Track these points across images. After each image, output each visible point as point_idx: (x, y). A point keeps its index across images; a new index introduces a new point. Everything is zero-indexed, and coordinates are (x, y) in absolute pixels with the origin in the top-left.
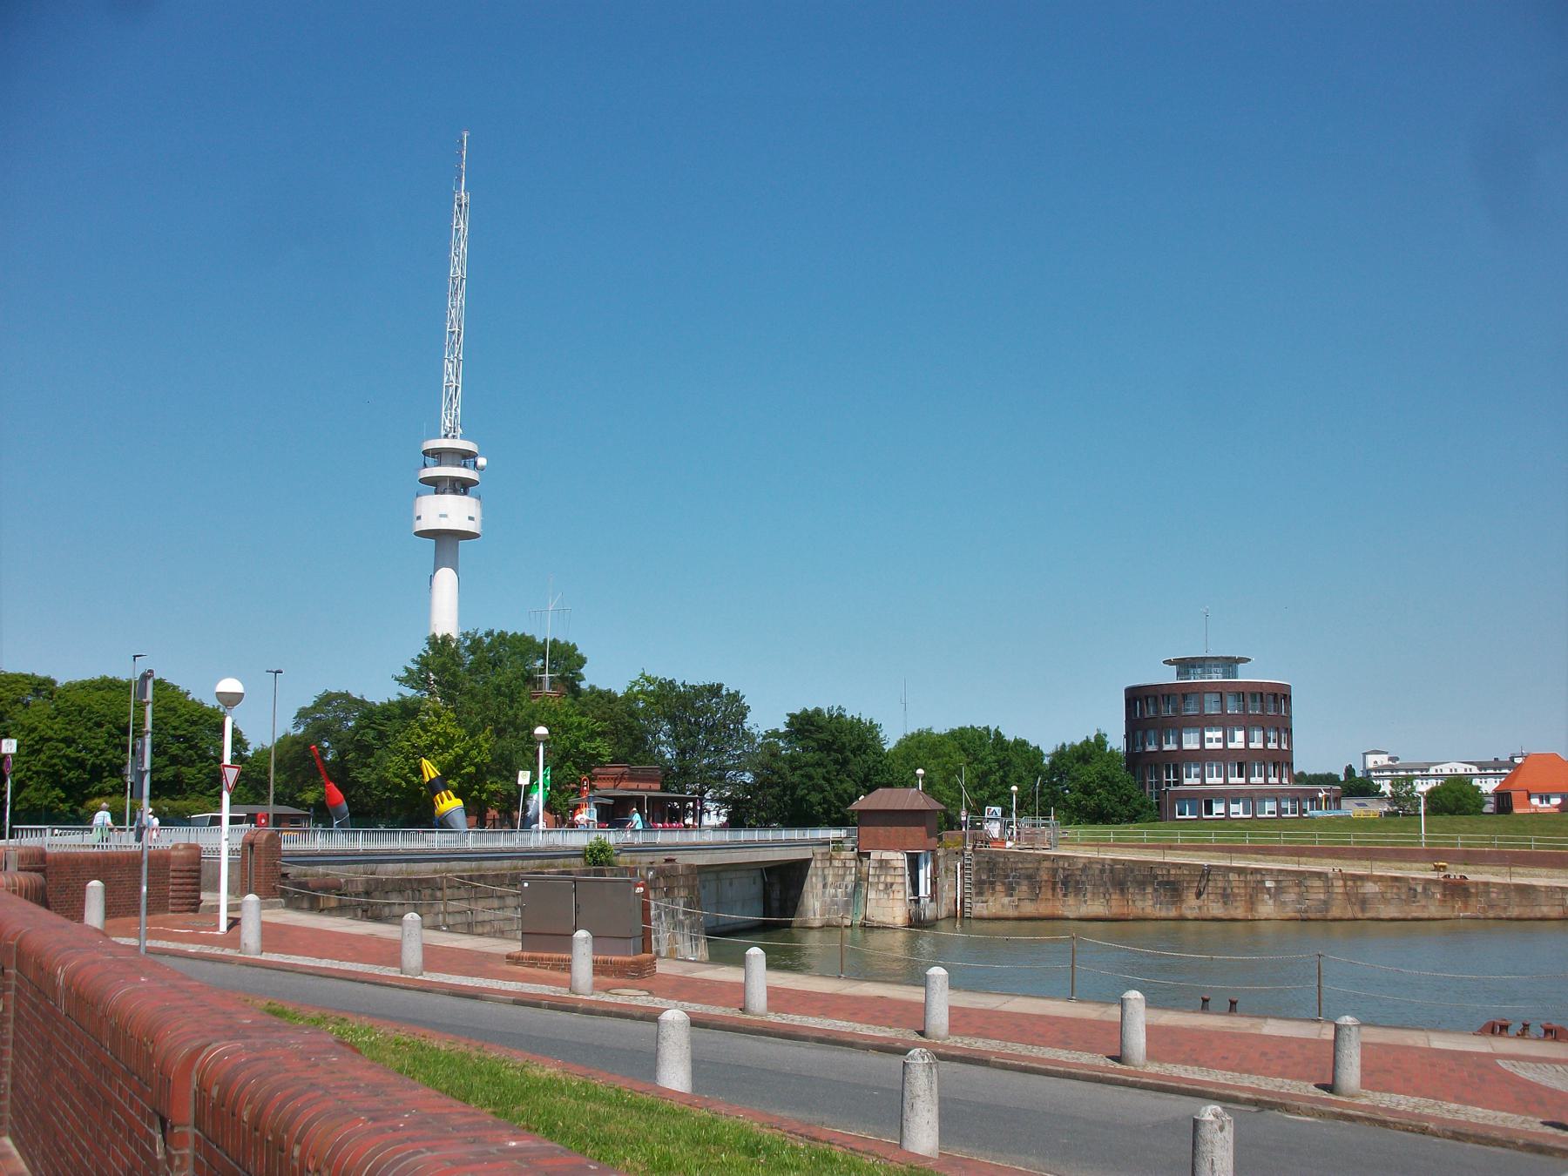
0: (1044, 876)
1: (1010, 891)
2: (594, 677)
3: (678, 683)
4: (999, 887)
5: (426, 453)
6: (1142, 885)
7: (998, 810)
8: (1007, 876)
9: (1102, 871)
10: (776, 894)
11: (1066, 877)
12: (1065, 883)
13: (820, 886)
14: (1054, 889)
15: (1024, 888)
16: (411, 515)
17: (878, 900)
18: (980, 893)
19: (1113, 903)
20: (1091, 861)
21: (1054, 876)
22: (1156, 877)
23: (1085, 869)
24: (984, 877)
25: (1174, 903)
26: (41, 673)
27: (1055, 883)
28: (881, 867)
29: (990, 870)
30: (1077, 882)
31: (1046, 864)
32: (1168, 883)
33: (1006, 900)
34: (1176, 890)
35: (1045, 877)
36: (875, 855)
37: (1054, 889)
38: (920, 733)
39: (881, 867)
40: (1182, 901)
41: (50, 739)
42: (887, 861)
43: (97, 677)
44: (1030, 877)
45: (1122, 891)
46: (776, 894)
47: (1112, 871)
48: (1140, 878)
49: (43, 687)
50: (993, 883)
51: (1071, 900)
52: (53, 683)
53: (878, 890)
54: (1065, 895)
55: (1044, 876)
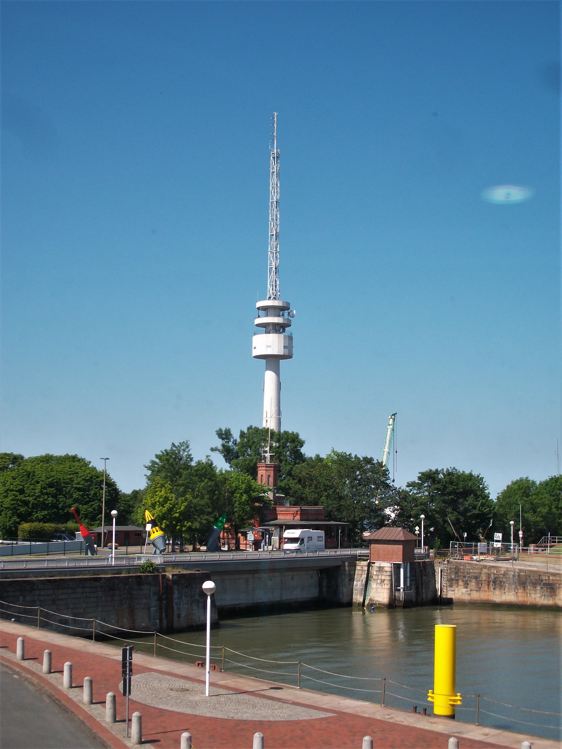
0: (484, 577)
1: (466, 585)
2: (308, 451)
3: (353, 456)
4: (461, 583)
5: (258, 309)
6: (534, 584)
7: (500, 535)
8: (464, 577)
9: (514, 576)
10: (325, 583)
11: (495, 578)
12: (494, 582)
13: (347, 580)
14: (488, 585)
15: (473, 584)
16: (249, 346)
17: (377, 588)
18: (451, 586)
19: (519, 594)
20: (508, 570)
21: (489, 578)
22: (542, 581)
23: (505, 574)
24: (453, 577)
25: (551, 596)
26: (16, 453)
27: (489, 582)
28: (379, 571)
29: (456, 573)
30: (501, 582)
31: (485, 571)
32: (549, 584)
33: (464, 590)
34: (553, 589)
35: (484, 578)
36: (377, 564)
37: (488, 585)
38: (521, 480)
39: (379, 571)
40: (555, 595)
41: (12, 490)
42: (383, 567)
43: (44, 454)
44: (476, 578)
45: (524, 587)
46: (325, 583)
47: (519, 576)
48: (534, 581)
49: (16, 459)
50: (457, 580)
51: (497, 592)
52: (22, 458)
53: (377, 583)
54: (494, 589)
55: (484, 577)
